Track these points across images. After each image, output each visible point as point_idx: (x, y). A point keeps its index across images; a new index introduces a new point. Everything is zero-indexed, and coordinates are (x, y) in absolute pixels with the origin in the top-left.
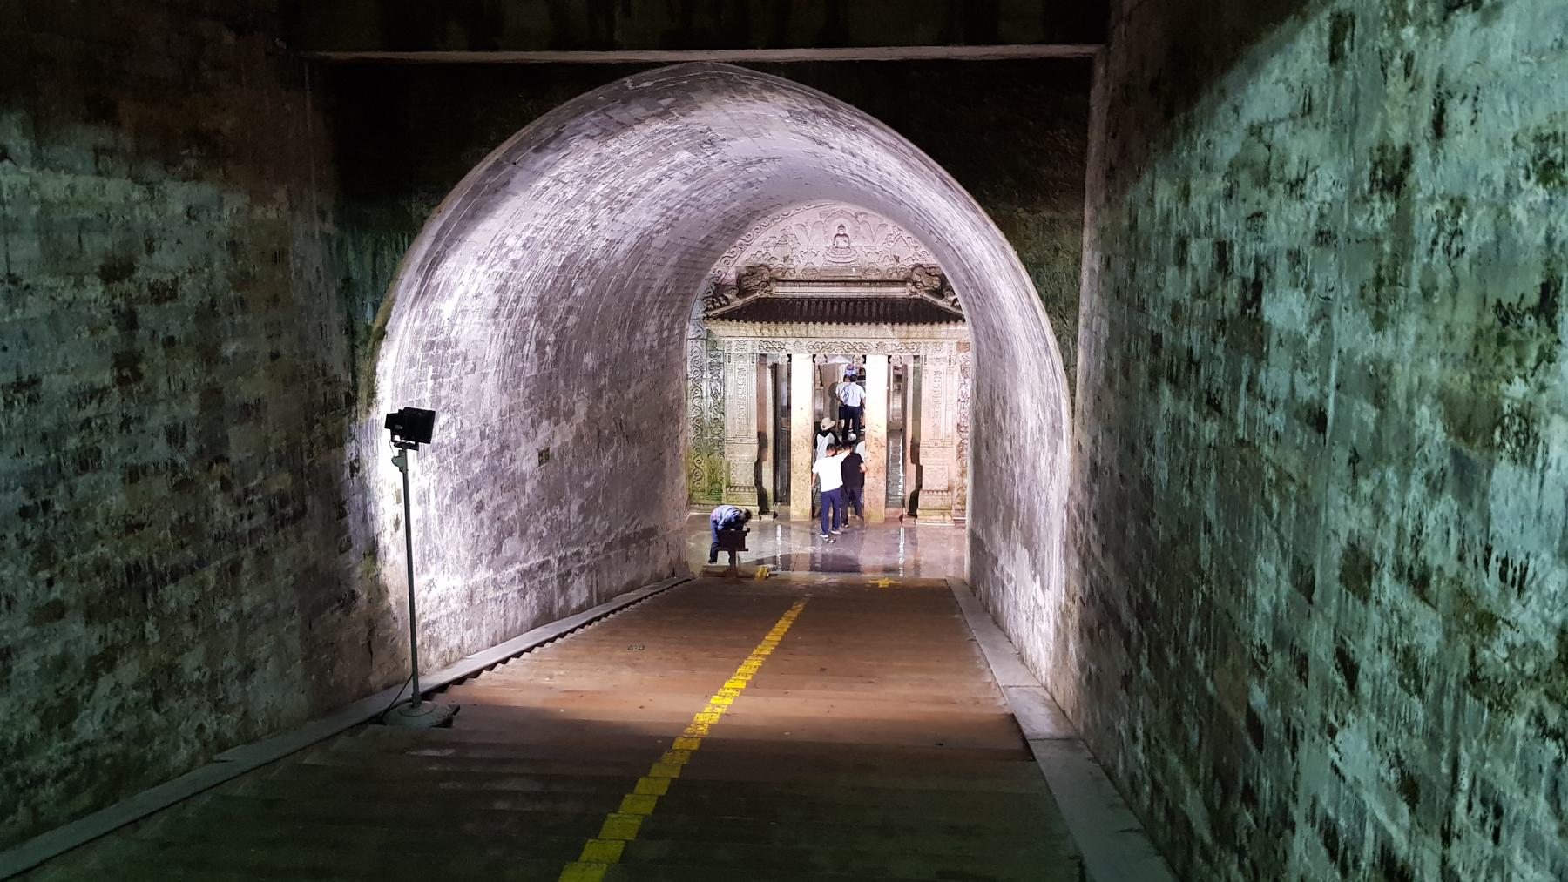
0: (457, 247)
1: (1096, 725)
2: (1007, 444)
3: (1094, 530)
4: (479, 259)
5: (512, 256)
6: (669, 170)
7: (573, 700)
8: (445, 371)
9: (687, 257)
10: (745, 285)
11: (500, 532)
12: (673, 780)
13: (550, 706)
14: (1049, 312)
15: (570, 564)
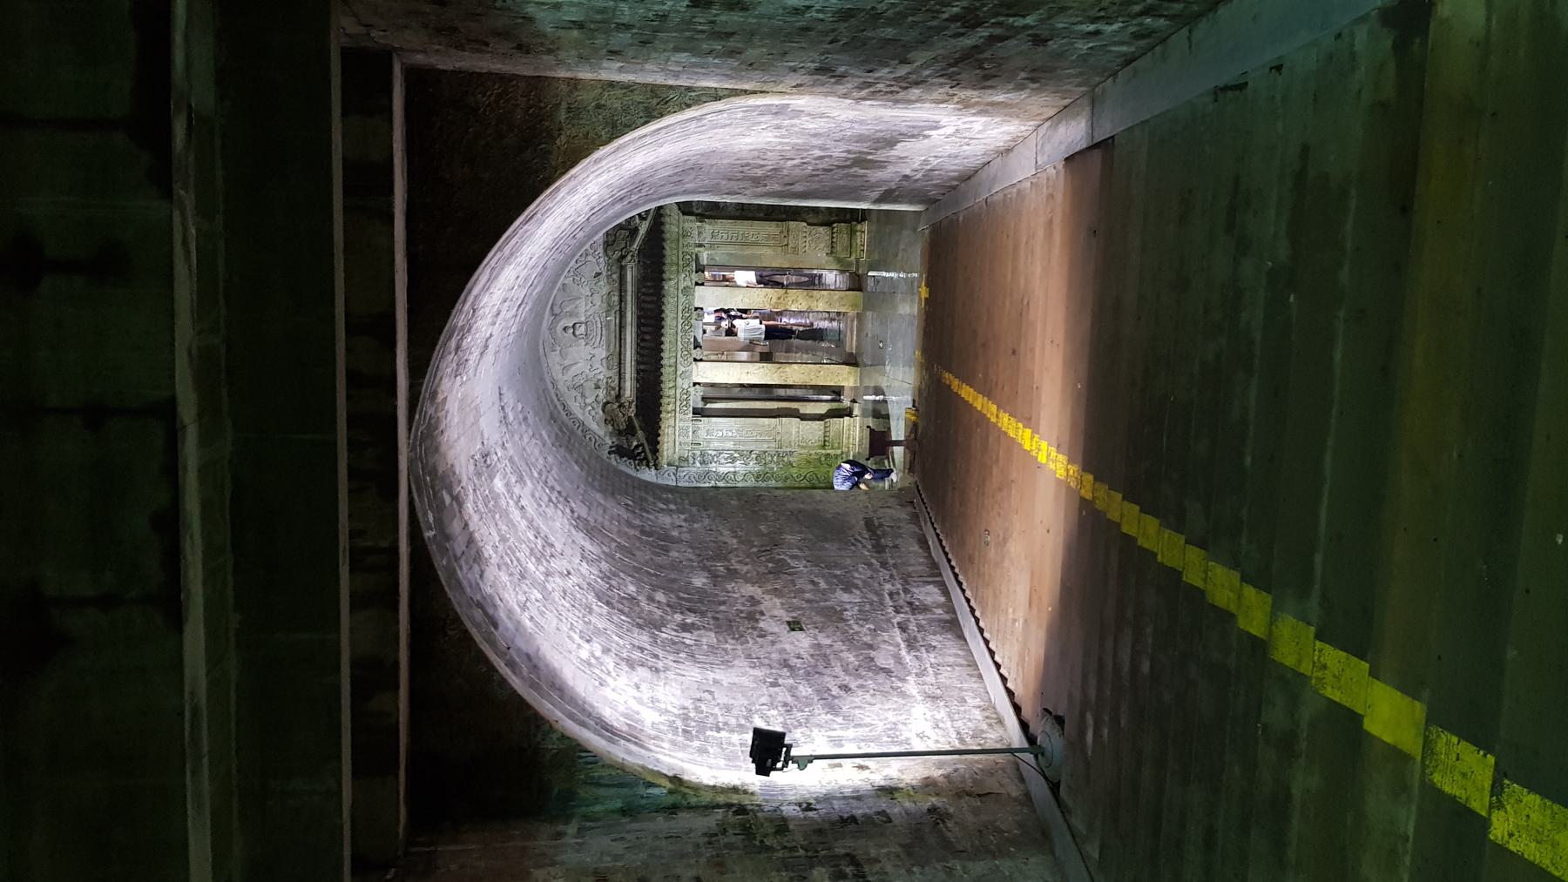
0: (592, 707)
1: (1081, 74)
2: (790, 163)
3: (883, 72)
4: (601, 684)
5: (598, 653)
6: (512, 498)
7: (1040, 598)
8: (711, 720)
9: (596, 483)
10: (623, 427)
11: (870, 669)
12: (1124, 498)
13: (1045, 621)
14: (662, 115)
15: (901, 602)
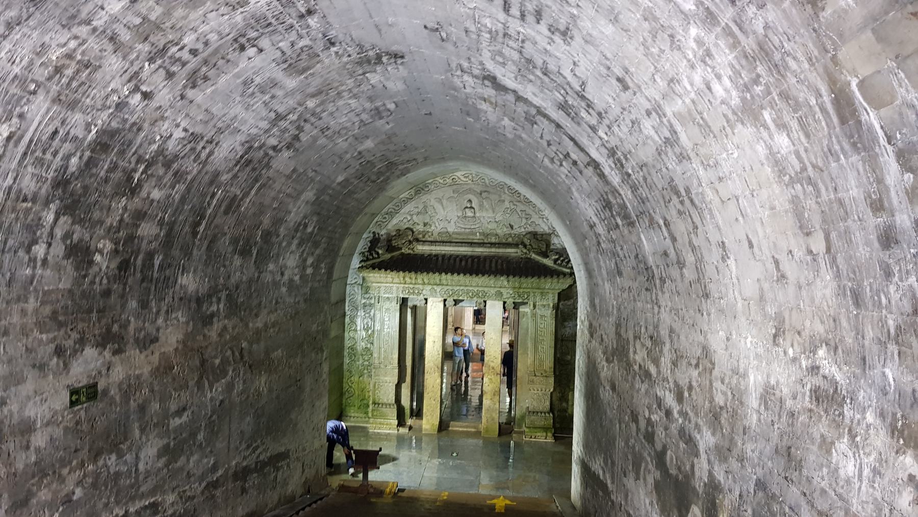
10: (394, 243)
